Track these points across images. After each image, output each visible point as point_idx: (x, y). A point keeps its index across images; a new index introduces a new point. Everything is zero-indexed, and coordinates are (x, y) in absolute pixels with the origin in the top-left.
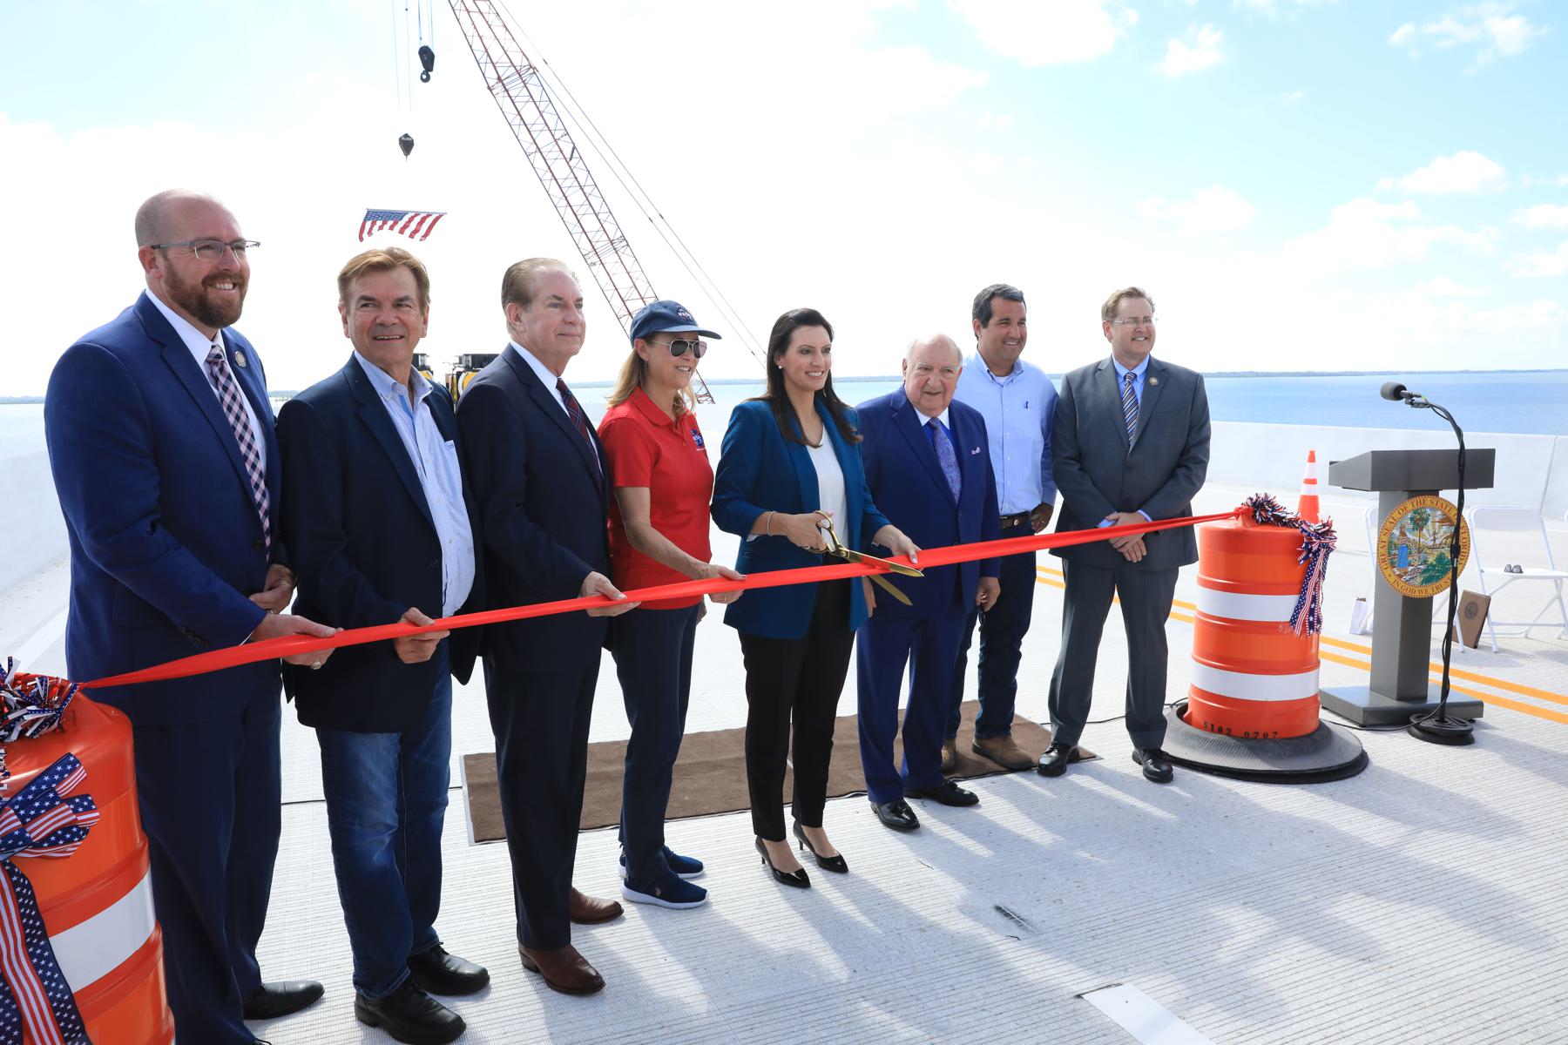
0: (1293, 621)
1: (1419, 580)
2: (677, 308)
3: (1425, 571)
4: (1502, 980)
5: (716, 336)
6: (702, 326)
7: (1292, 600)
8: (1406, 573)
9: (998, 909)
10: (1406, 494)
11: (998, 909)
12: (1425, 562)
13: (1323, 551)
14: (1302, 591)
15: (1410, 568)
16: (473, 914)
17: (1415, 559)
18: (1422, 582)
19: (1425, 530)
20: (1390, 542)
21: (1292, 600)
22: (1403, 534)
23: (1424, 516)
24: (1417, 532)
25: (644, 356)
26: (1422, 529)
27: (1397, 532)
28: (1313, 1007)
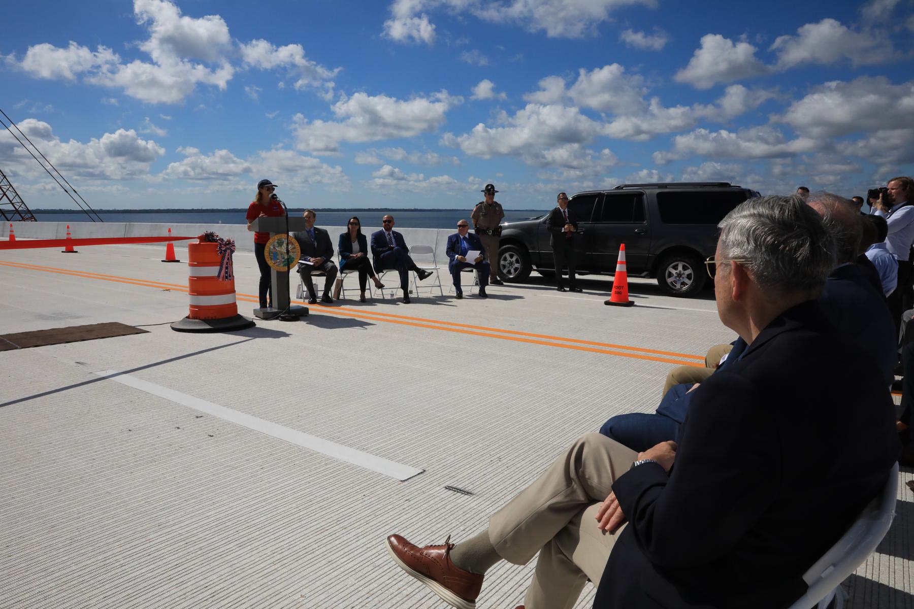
0: (219, 276)
1: (282, 265)
2: (268, 181)
3: (284, 262)
4: (388, 560)
5: (276, 186)
6: (273, 184)
7: (217, 268)
8: (277, 262)
9: (449, 488)
10: (274, 233)
11: (449, 488)
12: (284, 258)
13: (228, 251)
14: (221, 265)
15: (278, 261)
16: (337, 497)
17: (279, 257)
18: (283, 266)
19: (283, 247)
20: (270, 251)
21: (217, 268)
22: (274, 248)
23: (282, 241)
24: (280, 247)
25: (261, 192)
26: (281, 246)
27: (272, 247)
28: (96, 584)
